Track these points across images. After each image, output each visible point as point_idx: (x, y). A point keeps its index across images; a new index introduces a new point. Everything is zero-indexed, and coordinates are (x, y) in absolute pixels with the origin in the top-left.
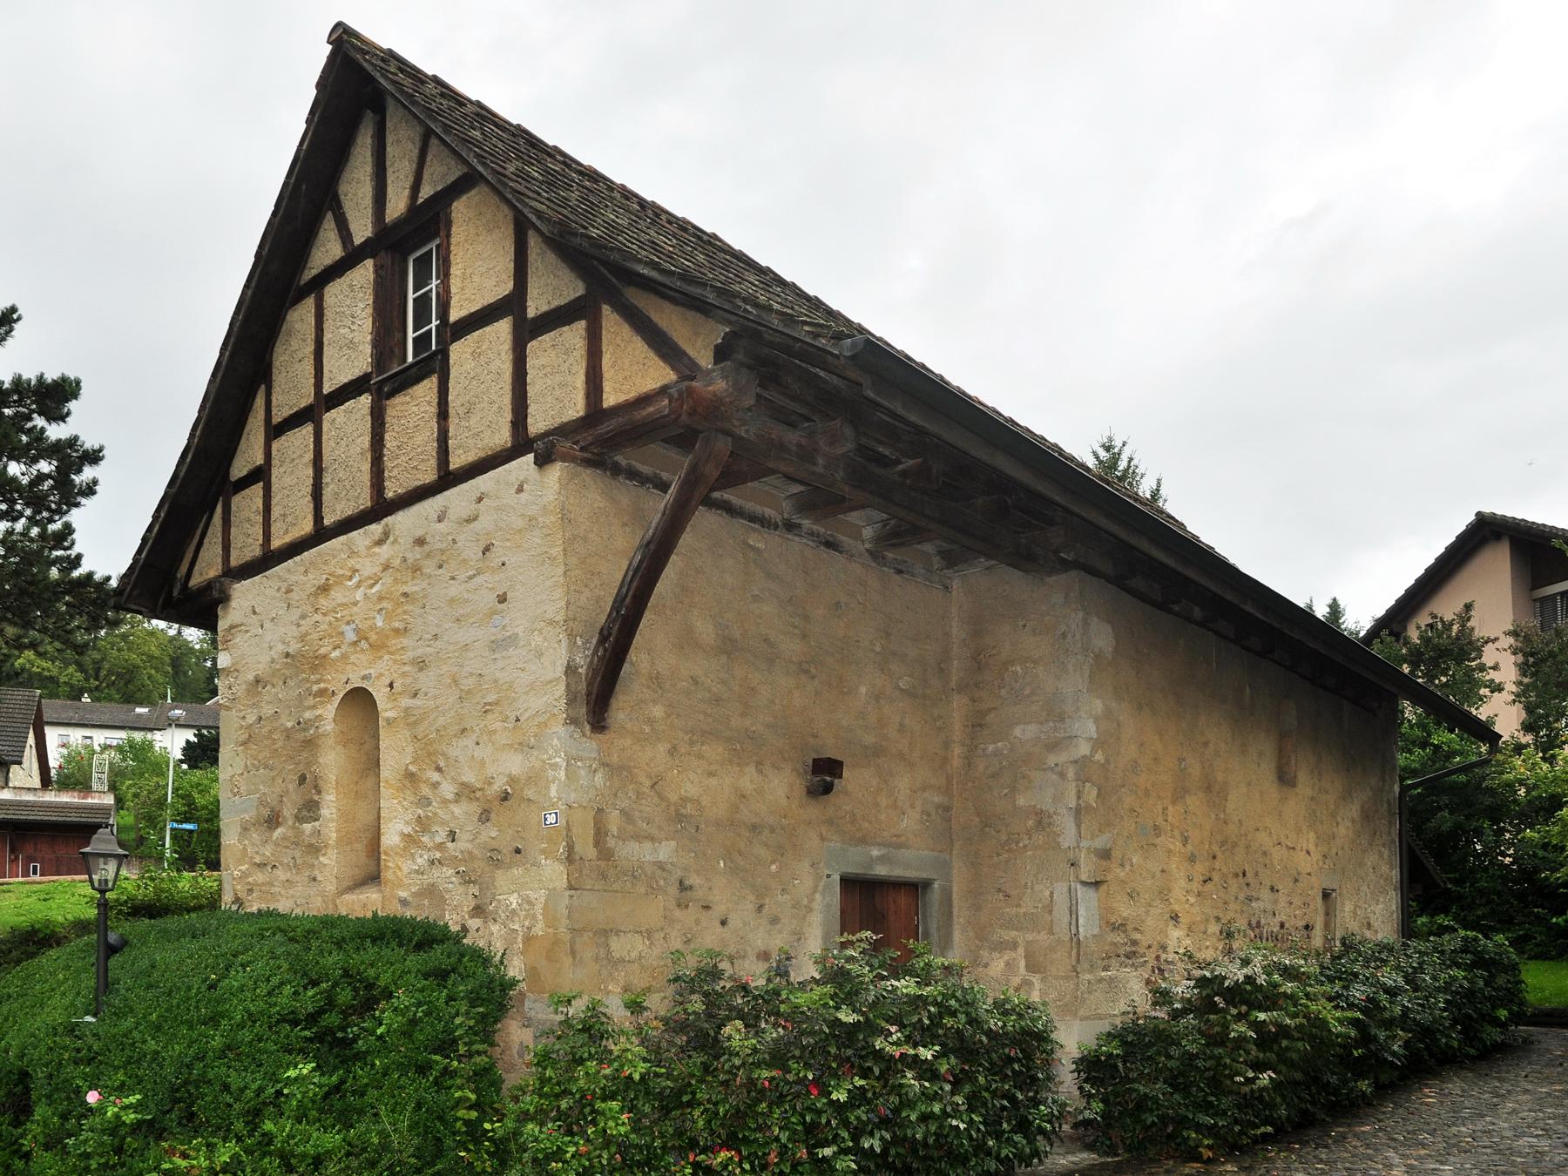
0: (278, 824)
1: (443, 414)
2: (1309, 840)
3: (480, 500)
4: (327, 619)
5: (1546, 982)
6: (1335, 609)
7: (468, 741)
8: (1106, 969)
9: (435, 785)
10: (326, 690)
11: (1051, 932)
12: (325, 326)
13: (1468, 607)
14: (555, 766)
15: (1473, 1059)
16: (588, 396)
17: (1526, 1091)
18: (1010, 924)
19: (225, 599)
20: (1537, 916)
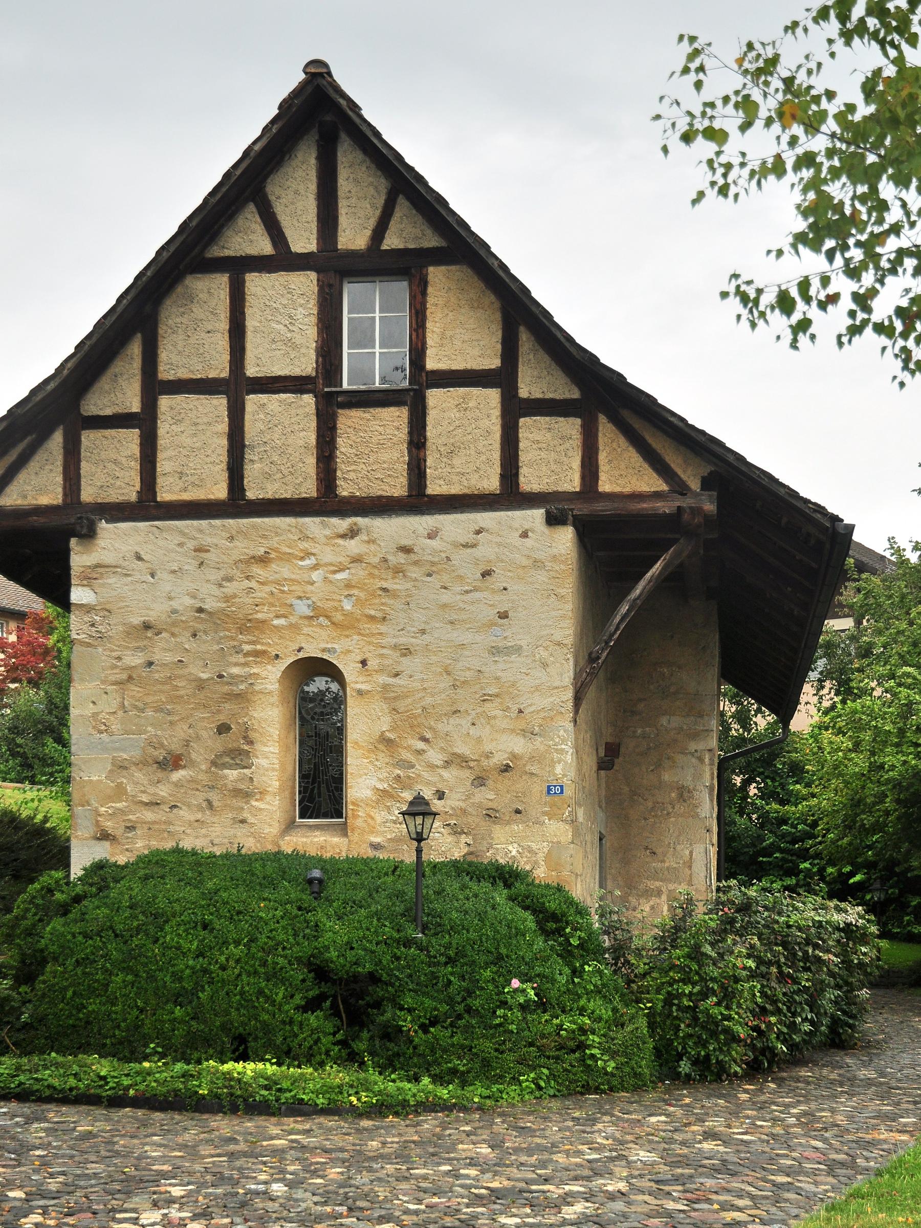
3: (478, 532)
10: (264, 652)
11: (690, 883)
18: (655, 876)
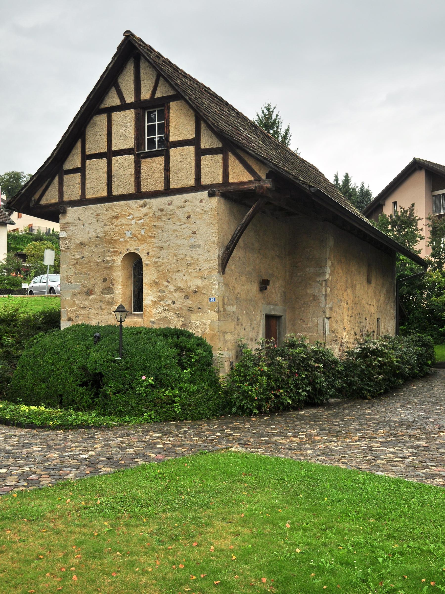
0: (91, 294)
1: (167, 169)
2: (374, 302)
3: (185, 202)
4: (118, 228)
5: (442, 352)
6: (347, 179)
7: (181, 274)
8: (331, 345)
9: (167, 286)
11: (317, 333)
12: (113, 127)
13: (413, 205)
14: (214, 285)
15: (422, 377)
16: (223, 177)
17: (439, 385)
19: (64, 212)
20: (434, 328)
